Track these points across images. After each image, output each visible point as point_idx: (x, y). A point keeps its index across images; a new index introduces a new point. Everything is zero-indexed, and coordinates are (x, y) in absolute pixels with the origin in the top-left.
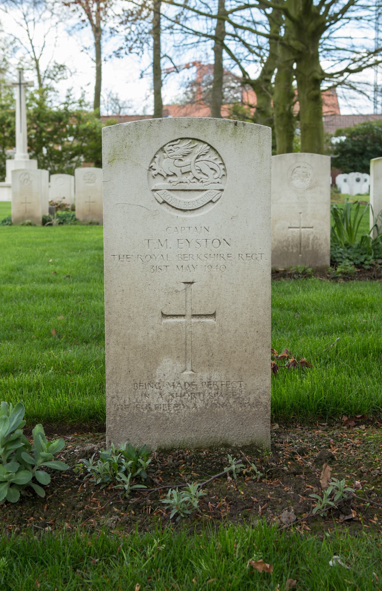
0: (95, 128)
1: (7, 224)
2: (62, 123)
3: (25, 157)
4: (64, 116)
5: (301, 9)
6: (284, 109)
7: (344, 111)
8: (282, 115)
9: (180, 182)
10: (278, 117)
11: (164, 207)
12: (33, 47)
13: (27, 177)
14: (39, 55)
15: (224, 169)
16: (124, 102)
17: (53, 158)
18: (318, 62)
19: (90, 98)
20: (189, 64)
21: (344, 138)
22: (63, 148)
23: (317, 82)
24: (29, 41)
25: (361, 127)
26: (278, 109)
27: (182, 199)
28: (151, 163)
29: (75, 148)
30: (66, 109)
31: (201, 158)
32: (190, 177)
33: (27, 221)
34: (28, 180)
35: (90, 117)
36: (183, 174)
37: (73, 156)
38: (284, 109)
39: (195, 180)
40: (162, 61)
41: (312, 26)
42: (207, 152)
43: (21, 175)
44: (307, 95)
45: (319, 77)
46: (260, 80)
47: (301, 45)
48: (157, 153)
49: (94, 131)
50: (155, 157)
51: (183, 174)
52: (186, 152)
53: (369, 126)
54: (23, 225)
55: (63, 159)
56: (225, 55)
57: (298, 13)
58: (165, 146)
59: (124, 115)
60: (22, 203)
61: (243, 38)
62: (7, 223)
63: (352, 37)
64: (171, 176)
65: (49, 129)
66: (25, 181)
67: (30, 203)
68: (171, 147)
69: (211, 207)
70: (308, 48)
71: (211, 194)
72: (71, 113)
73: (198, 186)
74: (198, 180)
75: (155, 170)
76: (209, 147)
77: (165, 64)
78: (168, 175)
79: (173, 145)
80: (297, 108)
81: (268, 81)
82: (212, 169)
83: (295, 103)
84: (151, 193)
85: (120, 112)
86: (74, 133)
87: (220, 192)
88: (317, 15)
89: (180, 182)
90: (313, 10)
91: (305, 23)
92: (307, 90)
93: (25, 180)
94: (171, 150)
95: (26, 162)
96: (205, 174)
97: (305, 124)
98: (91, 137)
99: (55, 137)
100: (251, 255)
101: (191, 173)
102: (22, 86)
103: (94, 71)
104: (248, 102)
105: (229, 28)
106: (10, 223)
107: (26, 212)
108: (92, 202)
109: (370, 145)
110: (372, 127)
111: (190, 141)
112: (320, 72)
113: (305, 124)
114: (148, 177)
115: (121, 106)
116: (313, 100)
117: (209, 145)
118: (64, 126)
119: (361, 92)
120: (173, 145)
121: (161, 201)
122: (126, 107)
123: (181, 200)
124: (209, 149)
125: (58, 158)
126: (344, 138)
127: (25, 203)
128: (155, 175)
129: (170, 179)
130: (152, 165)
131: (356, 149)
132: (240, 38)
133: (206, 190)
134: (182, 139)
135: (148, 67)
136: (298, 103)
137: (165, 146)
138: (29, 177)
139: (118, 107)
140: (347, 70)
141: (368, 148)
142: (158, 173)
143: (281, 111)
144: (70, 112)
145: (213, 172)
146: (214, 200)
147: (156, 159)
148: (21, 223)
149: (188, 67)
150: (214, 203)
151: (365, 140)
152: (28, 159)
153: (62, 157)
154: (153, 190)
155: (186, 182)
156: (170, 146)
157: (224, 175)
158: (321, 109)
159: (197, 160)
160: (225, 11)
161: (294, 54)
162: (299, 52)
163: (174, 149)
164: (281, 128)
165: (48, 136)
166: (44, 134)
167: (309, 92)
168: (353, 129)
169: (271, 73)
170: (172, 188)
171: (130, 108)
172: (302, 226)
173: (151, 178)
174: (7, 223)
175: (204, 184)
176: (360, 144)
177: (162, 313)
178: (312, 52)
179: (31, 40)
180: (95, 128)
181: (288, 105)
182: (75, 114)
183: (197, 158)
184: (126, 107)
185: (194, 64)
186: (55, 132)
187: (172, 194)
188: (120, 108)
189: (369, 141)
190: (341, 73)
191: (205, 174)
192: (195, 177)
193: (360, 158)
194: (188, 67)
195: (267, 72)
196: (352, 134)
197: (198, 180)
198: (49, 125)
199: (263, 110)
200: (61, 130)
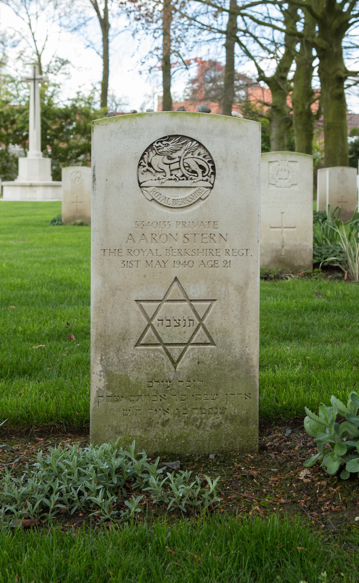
1: (58, 224)
3: (38, 155)
5: (325, 6)
6: (304, 108)
8: (301, 113)
10: (297, 115)
11: (153, 204)
12: (35, 41)
13: (78, 175)
14: (41, 50)
16: (120, 101)
17: (58, 156)
23: (341, 80)
26: (297, 108)
29: (81, 146)
33: (79, 221)
34: (79, 178)
37: (78, 155)
38: (304, 108)
41: (335, 23)
43: (72, 173)
44: (331, 93)
45: (343, 75)
46: (276, 77)
54: (75, 224)
55: (69, 157)
57: (321, 10)
58: (154, 142)
59: (120, 112)
60: (73, 202)
61: (254, 34)
62: (57, 223)
65: (54, 127)
66: (77, 180)
67: (81, 202)
69: (202, 203)
71: (200, 191)
80: (314, 107)
81: (284, 78)
83: (314, 101)
85: (116, 109)
86: (82, 131)
88: (341, 13)
90: (336, 7)
91: (329, 20)
92: (330, 88)
93: (76, 179)
95: (40, 160)
97: (328, 123)
100: (237, 251)
102: (37, 81)
103: (101, 68)
104: (264, 101)
105: (241, 25)
106: (60, 223)
107: (77, 211)
108: (344, 202)
112: (343, 69)
113: (328, 123)
115: (117, 103)
116: (336, 98)
121: (150, 198)
122: (123, 104)
125: (63, 156)
127: (76, 202)
132: (251, 35)
136: (317, 101)
138: (81, 176)
139: (114, 104)
143: (300, 109)
146: (203, 197)
148: (73, 223)
152: (41, 158)
153: (67, 155)
159: (186, 157)
160: (237, 7)
164: (300, 127)
165: (53, 133)
166: (49, 131)
167: (333, 90)
169: (287, 70)
171: (127, 105)
172: (284, 225)
174: (57, 223)
175: (161, 181)
178: (335, 50)
179: (33, 34)
181: (308, 103)
182: (84, 111)
184: (123, 104)
187: (162, 191)
188: (117, 105)
192: (183, 175)
195: (283, 70)
198: (55, 122)
199: (279, 108)
200: (67, 127)
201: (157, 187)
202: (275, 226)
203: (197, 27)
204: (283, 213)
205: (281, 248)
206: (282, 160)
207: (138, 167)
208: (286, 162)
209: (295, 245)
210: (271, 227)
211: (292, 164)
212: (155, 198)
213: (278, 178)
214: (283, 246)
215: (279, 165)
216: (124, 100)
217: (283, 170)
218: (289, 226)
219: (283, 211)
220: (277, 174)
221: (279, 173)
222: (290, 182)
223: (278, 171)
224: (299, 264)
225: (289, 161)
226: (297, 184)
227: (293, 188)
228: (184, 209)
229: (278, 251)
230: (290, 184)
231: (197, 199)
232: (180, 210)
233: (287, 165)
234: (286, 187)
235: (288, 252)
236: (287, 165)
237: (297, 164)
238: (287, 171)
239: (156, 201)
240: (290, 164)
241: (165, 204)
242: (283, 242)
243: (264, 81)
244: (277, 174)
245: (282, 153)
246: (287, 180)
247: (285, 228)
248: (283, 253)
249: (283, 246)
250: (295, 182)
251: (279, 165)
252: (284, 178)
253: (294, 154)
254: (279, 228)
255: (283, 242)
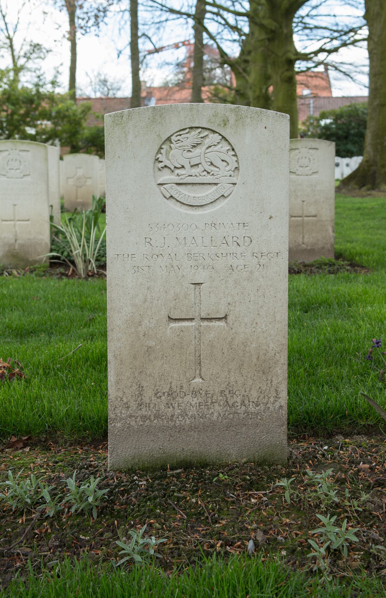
0: (67, 110)
2: (34, 106)
4: (36, 98)
6: (261, 91)
7: (336, 93)
9: (189, 176)
10: (254, 99)
12: (6, 24)
14: (13, 33)
15: (236, 161)
18: (291, 42)
19: (64, 79)
20: (178, 43)
21: (328, 121)
22: (37, 132)
23: (291, 63)
24: (2, 18)
25: (345, 109)
27: (187, 193)
28: (157, 153)
29: (48, 132)
30: (38, 91)
31: (210, 150)
32: (200, 169)
35: (62, 99)
36: (192, 166)
38: (261, 91)
39: (205, 173)
40: (140, 41)
42: (218, 143)
45: (293, 57)
47: (275, 24)
48: (163, 144)
49: (67, 113)
50: (161, 148)
51: (192, 166)
52: (196, 141)
53: (353, 108)
56: (205, 35)
58: (172, 135)
63: (336, 14)
64: (178, 168)
68: (179, 137)
69: (223, 203)
70: (281, 27)
72: (43, 95)
73: (208, 179)
74: (208, 173)
75: (161, 162)
76: (221, 137)
77: (144, 45)
78: (175, 167)
79: (180, 135)
82: (223, 160)
84: (156, 187)
87: (232, 185)
89: (189, 176)
94: (179, 140)
96: (215, 166)
98: (65, 120)
99: (28, 119)
101: (200, 165)
109: (354, 128)
110: (357, 110)
111: (200, 130)
112: (294, 52)
114: (154, 171)
115: (109, 87)
116: (286, 81)
117: (220, 135)
118: (36, 109)
119: (345, 73)
120: (180, 135)
121: (168, 195)
123: (185, 193)
124: (221, 140)
126: (328, 121)
128: (162, 167)
129: (177, 171)
130: (157, 157)
131: (340, 132)
133: (216, 184)
134: (191, 128)
135: (125, 48)
137: (172, 135)
140: (321, 50)
141: (352, 132)
142: (166, 166)
143: (257, 93)
144: (42, 93)
145: (225, 164)
146: (226, 195)
147: (162, 151)
149: (177, 46)
150: (226, 197)
151: (350, 122)
154: (159, 184)
155: (196, 176)
156: (177, 136)
157: (236, 168)
158: (295, 91)
159: (207, 151)
161: (266, 33)
162: (272, 31)
163: (181, 140)
167: (283, 73)
168: (338, 110)
170: (180, 182)
172: (17, 218)
173: (156, 170)
176: (344, 127)
177: (169, 317)
178: (285, 31)
180: (67, 110)
181: (265, 87)
183: (208, 148)
185: (184, 43)
186: (27, 114)
187: (181, 189)
189: (353, 124)
190: (316, 53)
191: (215, 166)
192: (205, 170)
193: (345, 142)
194: (177, 46)
195: (246, 53)
196: (337, 117)
197: (208, 173)
198: (21, 107)
199: (242, 92)
201: (177, 184)
202: (7, 219)
203: (158, 9)
204: (15, 205)
205: (14, 242)
206: (12, 149)
207: (155, 162)
208: (17, 152)
209: (29, 239)
210: (3, 220)
211: (24, 154)
212: (173, 196)
213: (9, 168)
214: (16, 240)
215: (9, 154)
216: (115, 85)
217: (14, 160)
218: (22, 219)
219: (15, 204)
220: (8, 164)
221: (299, 160)
222: (21, 172)
223: (8, 161)
224: (33, 258)
225: (20, 151)
226: (29, 175)
227: (25, 179)
228: (201, 209)
229: (10, 245)
230: (22, 175)
231: (219, 196)
232: (186, 207)
233: (18, 155)
234: (17, 178)
235: (22, 246)
236: (18, 155)
237: (29, 154)
238: (307, 158)
239: (174, 198)
240: (21, 153)
241: (185, 202)
242: (16, 235)
243: (228, 64)
244: (8, 164)
245: (12, 142)
246: (18, 171)
247: (18, 220)
248: (17, 247)
249: (16, 240)
250: (28, 173)
251: (9, 154)
252: (15, 168)
253: (25, 143)
254: (11, 220)
255: (16, 235)
